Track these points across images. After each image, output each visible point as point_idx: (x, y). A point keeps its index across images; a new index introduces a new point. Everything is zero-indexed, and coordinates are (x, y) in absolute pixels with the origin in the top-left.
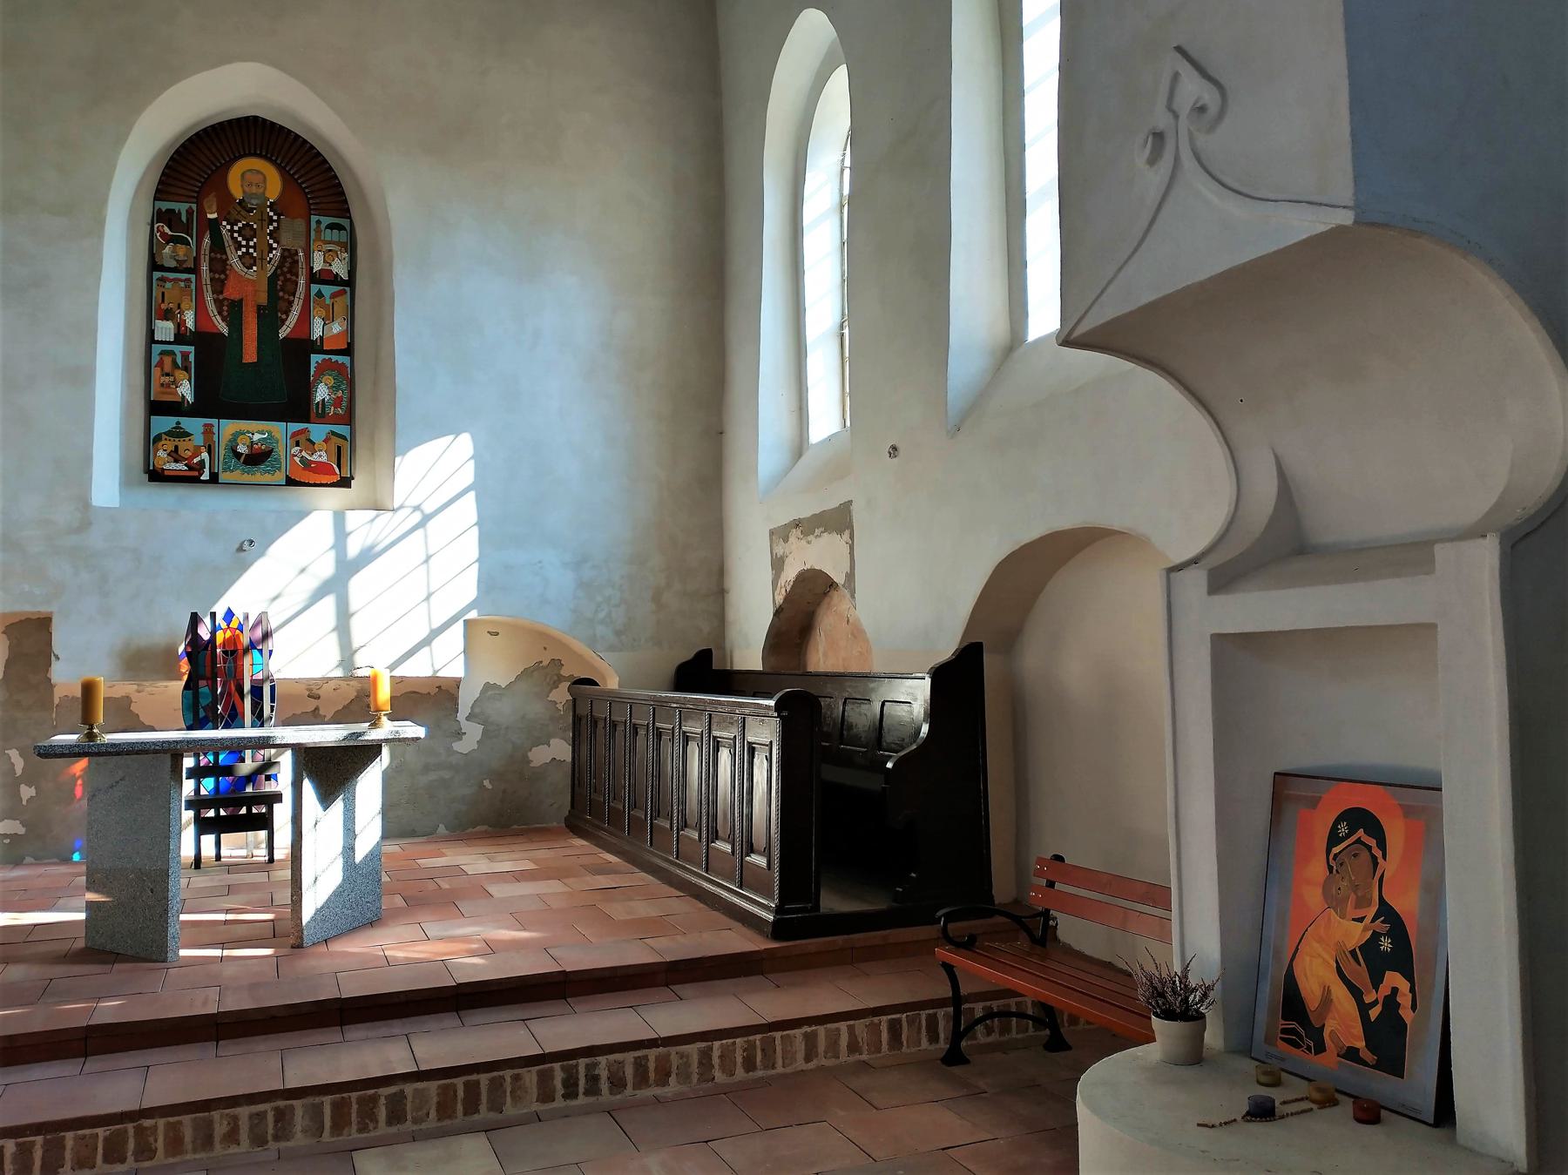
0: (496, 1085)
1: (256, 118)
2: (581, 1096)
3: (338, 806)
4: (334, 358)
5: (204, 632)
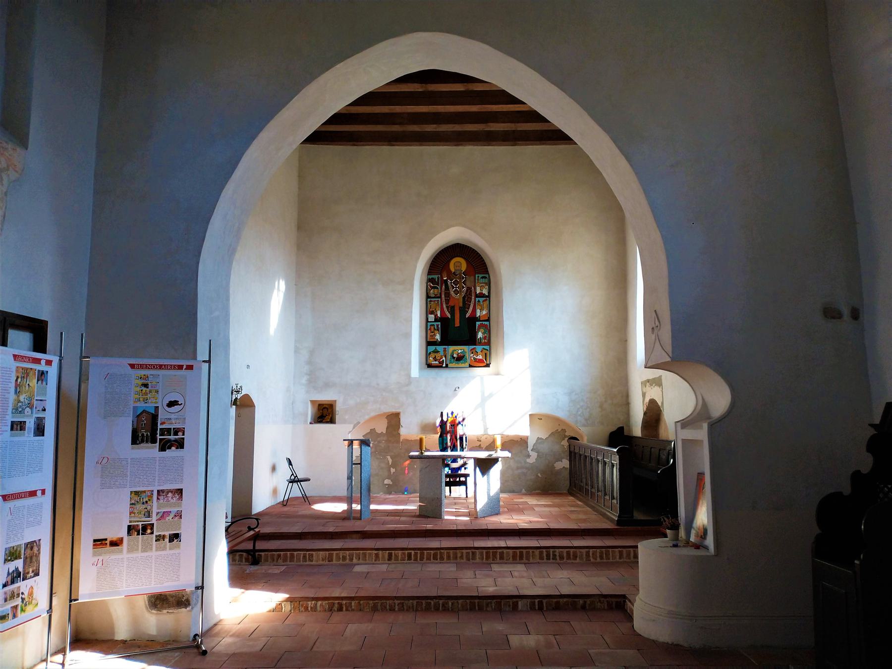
0: (528, 553)
1: (458, 244)
2: (551, 560)
3: (486, 476)
4: (484, 323)
5: (445, 419)
